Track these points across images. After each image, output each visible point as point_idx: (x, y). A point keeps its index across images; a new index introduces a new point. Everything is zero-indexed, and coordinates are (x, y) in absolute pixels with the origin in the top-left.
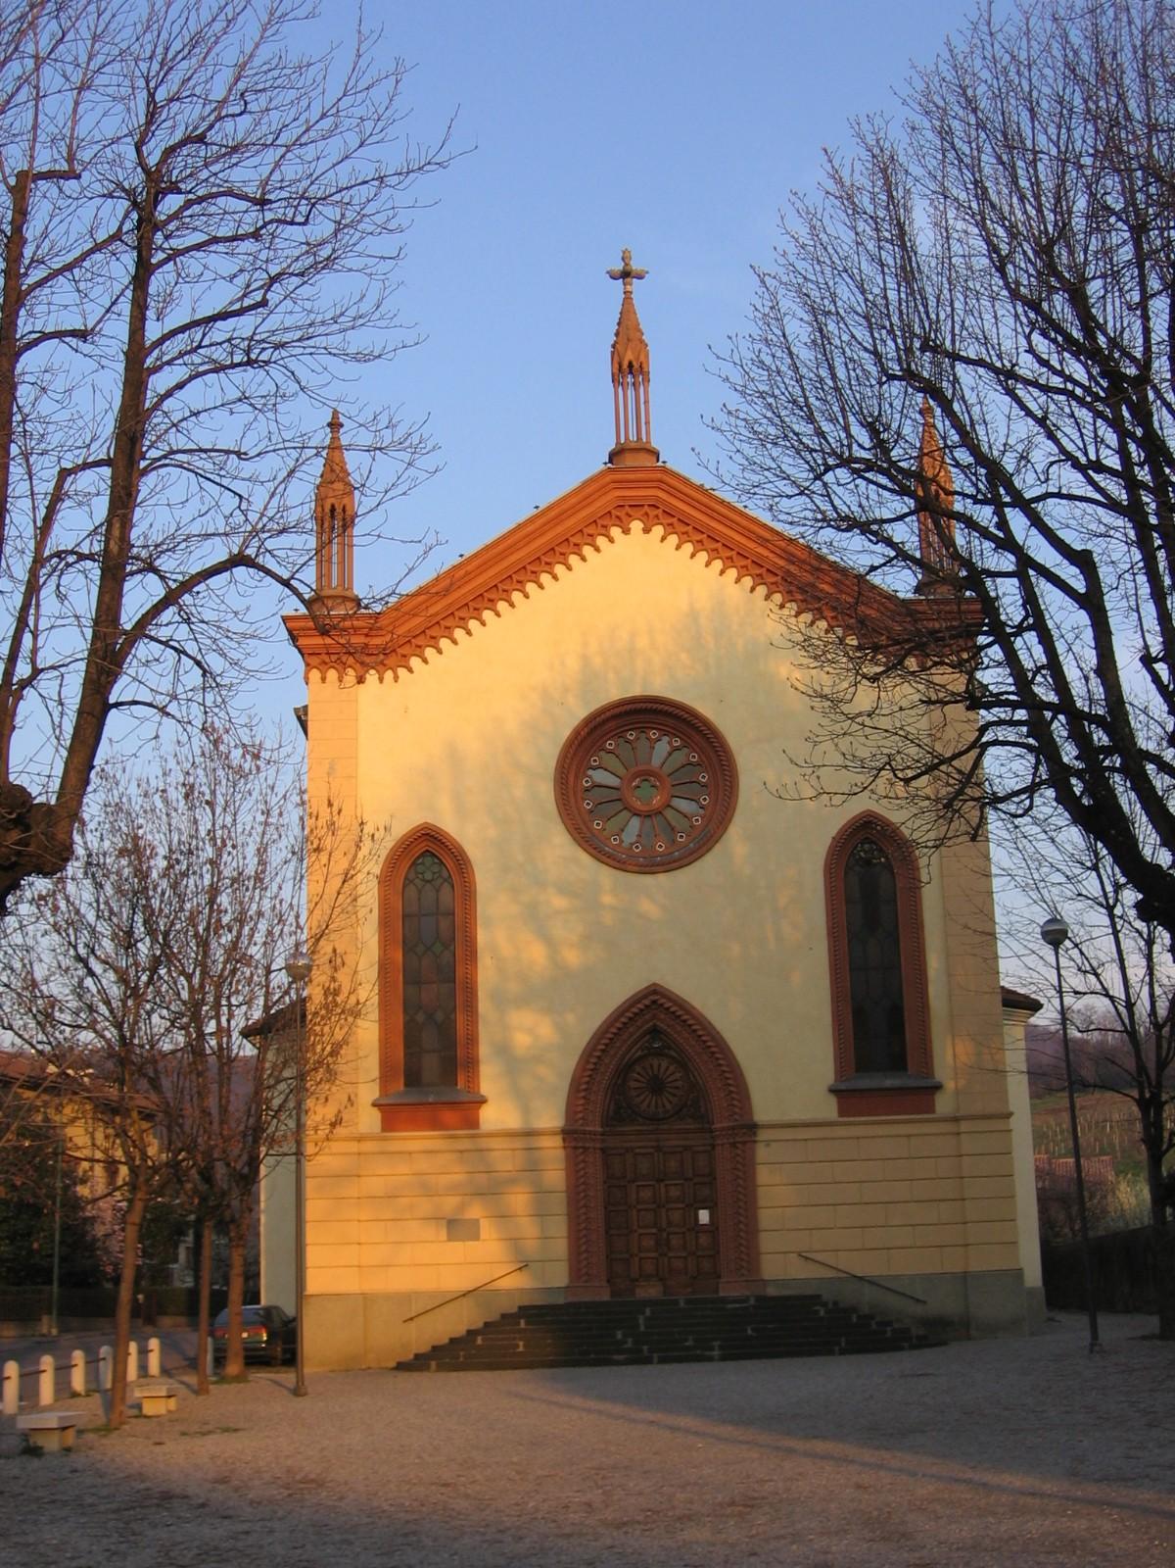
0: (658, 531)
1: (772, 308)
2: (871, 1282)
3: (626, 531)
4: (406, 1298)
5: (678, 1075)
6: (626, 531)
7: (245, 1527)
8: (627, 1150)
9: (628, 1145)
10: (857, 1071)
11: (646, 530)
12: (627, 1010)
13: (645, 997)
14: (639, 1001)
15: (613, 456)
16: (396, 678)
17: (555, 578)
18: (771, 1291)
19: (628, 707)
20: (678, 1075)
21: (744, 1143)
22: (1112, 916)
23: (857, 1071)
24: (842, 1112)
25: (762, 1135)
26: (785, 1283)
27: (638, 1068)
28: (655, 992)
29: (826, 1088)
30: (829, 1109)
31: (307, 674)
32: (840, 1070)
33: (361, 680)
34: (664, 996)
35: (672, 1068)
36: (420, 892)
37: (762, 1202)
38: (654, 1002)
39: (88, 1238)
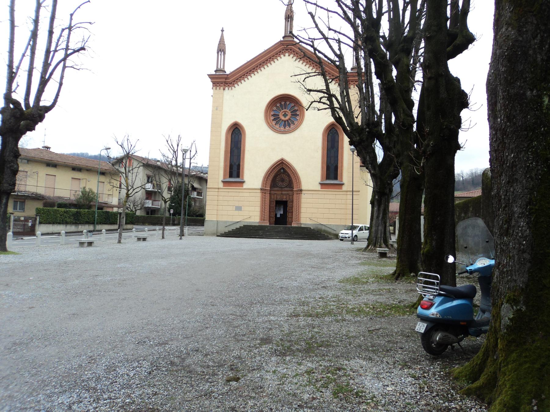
0: (292, 56)
1: (270, 376)
2: (324, 225)
3: (284, 56)
4: (226, 222)
5: (287, 178)
6: (284, 56)
7: (474, 7)
8: (275, 194)
9: (275, 192)
10: (326, 179)
11: (289, 55)
12: (275, 164)
13: (280, 161)
14: (279, 161)
15: (283, 37)
16: (232, 89)
17: (268, 66)
18: (302, 226)
19: (282, 96)
20: (287, 178)
21: (299, 194)
22: (353, 154)
23: (326, 179)
24: (321, 188)
25: (303, 192)
26: (305, 224)
27: (279, 176)
28: (282, 160)
29: (70, 14)
30: (319, 187)
31: (213, 87)
32: (322, 179)
33: (224, 89)
34: (284, 161)
35: (286, 177)
36: (235, 136)
37: (301, 217)
38: (282, 162)
39: (543, 100)
